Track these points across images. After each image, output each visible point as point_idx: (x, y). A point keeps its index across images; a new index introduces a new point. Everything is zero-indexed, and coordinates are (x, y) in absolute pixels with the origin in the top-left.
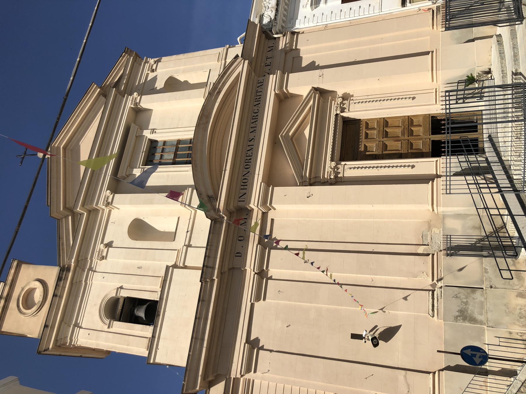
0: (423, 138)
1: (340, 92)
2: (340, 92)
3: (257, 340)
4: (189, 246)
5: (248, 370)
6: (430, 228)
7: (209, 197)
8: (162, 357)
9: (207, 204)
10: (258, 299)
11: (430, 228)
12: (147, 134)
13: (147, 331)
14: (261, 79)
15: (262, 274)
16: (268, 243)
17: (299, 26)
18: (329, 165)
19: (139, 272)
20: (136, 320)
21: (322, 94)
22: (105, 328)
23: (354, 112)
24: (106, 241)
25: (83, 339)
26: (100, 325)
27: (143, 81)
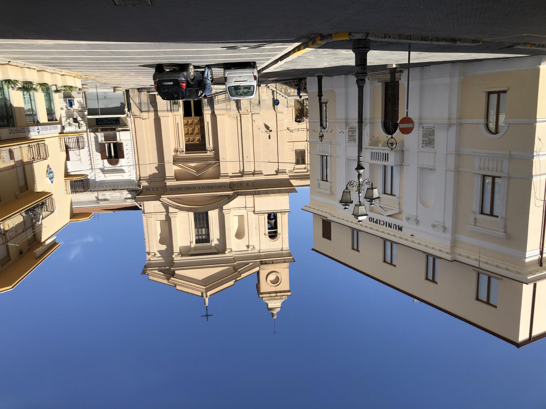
0: (194, 119)
1: (173, 153)
2: (173, 153)
3: (276, 171)
4: (246, 207)
5: (286, 172)
6: (231, 116)
7: (229, 198)
8: (287, 207)
9: (230, 198)
10: (262, 173)
11: (231, 116)
12: (194, 245)
13: (279, 215)
14: (168, 189)
15: (254, 174)
16: (243, 174)
17: (134, 177)
18: (209, 153)
19: (258, 228)
20: (276, 223)
21: (176, 161)
22: (281, 235)
23: (183, 147)
24: (247, 249)
25: (286, 246)
26: (280, 239)
27: (161, 258)
